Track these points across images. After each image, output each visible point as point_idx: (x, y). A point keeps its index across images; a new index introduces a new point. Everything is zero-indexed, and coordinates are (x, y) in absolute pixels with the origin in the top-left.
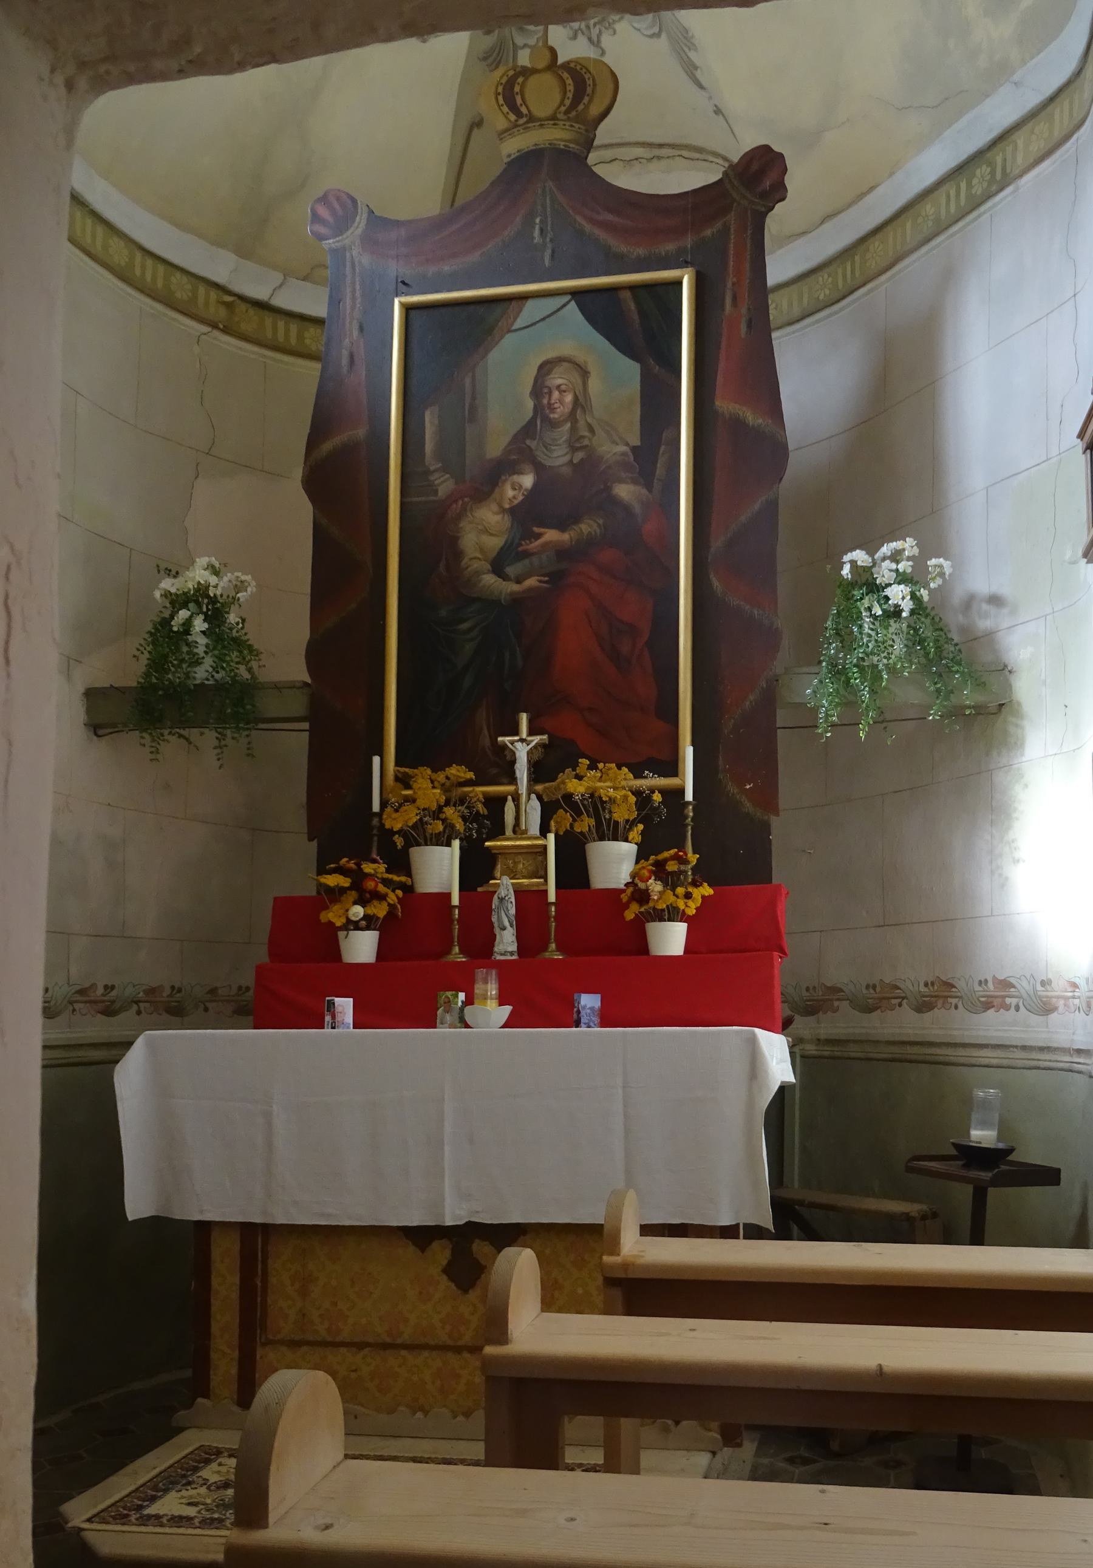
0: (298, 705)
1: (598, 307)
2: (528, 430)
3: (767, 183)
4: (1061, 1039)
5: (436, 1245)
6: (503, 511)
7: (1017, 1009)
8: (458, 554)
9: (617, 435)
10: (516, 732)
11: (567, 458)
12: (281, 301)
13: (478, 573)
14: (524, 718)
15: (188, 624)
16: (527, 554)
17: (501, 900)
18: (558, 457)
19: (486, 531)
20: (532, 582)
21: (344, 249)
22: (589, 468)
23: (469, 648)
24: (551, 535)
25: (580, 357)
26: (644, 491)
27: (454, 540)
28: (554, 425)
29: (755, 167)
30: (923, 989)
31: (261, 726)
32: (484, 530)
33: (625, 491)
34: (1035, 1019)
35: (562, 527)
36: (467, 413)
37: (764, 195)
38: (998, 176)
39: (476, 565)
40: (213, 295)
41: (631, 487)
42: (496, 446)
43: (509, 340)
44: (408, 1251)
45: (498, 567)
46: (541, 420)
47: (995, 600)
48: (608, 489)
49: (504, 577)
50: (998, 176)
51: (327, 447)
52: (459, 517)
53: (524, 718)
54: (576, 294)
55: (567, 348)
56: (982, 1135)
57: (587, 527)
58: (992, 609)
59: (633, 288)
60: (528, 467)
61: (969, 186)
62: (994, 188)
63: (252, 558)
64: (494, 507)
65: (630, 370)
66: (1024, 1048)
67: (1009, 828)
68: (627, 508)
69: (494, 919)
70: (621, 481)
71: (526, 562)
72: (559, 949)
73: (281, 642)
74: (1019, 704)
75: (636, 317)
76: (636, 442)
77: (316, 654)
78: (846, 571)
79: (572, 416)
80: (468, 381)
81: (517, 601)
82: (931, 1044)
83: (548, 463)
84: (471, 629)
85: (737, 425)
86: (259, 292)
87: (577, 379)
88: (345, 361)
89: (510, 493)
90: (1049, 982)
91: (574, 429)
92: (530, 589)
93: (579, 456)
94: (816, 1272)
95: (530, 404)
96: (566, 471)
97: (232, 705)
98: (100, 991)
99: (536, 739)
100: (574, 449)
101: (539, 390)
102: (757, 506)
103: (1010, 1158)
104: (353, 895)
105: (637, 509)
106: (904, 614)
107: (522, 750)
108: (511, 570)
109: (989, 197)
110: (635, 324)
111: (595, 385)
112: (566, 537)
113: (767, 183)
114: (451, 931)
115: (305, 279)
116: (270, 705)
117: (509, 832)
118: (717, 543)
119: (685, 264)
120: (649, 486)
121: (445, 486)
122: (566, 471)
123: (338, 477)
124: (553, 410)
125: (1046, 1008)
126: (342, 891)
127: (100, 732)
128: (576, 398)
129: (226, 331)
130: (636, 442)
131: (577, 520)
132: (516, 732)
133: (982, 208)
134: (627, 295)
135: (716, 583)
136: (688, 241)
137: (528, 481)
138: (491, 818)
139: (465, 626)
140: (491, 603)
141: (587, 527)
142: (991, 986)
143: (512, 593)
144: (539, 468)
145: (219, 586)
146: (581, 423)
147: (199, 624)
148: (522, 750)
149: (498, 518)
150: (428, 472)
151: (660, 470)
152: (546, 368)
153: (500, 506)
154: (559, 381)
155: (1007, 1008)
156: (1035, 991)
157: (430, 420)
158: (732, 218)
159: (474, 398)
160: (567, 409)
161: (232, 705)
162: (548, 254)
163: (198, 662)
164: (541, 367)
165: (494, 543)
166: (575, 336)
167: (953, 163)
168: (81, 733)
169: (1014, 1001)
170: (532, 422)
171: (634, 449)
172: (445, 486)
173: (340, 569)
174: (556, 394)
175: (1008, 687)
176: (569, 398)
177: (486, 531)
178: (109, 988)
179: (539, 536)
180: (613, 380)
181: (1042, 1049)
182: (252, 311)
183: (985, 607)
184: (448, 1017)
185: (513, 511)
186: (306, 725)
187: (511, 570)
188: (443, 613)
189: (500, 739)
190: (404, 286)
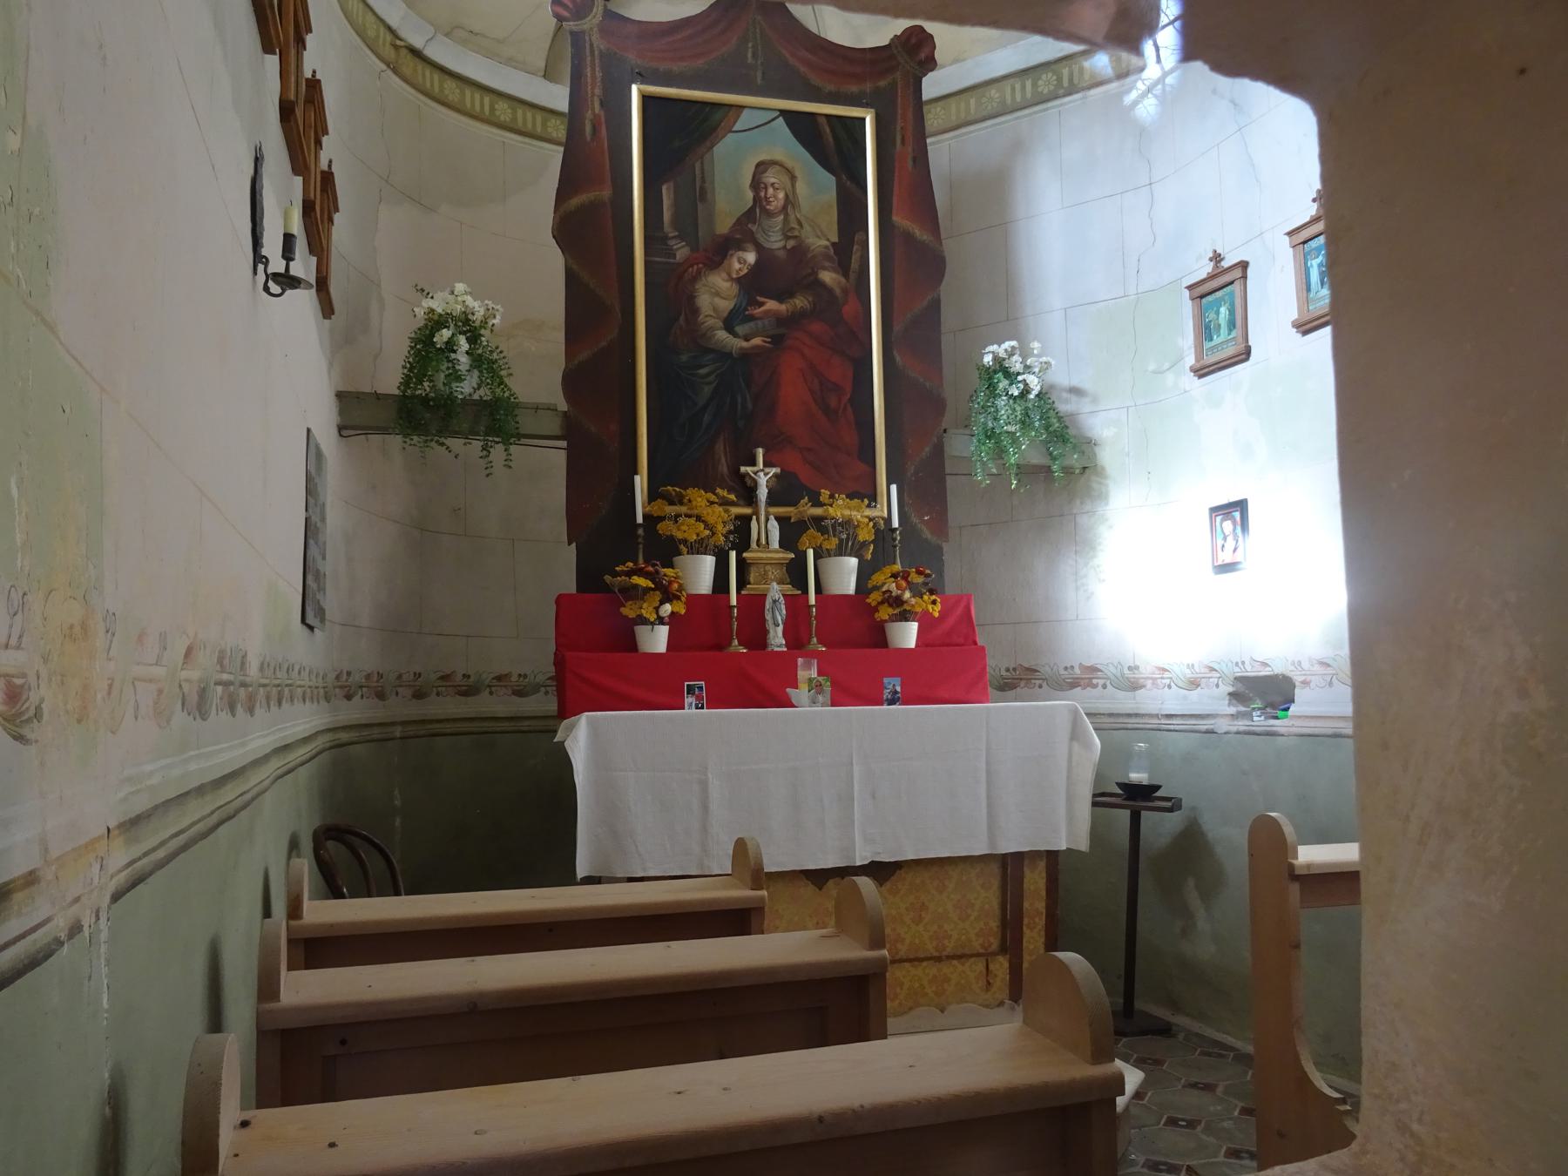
0: (553, 425)
1: (802, 126)
2: (749, 215)
3: (923, 56)
4: (1151, 708)
5: (831, 883)
6: (732, 279)
7: (1104, 686)
8: (695, 311)
9: (821, 234)
10: (753, 463)
11: (781, 244)
12: (432, 52)
13: (712, 329)
14: (760, 452)
15: (450, 346)
16: (752, 318)
17: (775, 601)
18: (775, 241)
19: (717, 294)
20: (757, 341)
21: (583, 32)
22: (798, 253)
23: (707, 390)
24: (771, 305)
25: (789, 163)
26: (843, 280)
27: (691, 298)
28: (770, 214)
29: (913, 40)
30: (1004, 673)
31: (523, 441)
32: (716, 294)
33: (828, 277)
34: (1121, 694)
35: (781, 301)
36: (696, 196)
37: (921, 63)
38: (1066, 84)
39: (711, 322)
40: (389, 37)
41: (834, 275)
42: (724, 226)
43: (730, 138)
44: (808, 890)
45: (729, 324)
46: (757, 211)
47: (1076, 391)
48: (815, 273)
49: (735, 335)
50: (1066, 84)
51: (575, 202)
52: (696, 278)
53: (760, 452)
54: (784, 113)
55: (778, 155)
56: (1138, 777)
57: (800, 302)
58: (1074, 398)
59: (828, 116)
60: (750, 246)
61: (1035, 85)
62: (1061, 92)
63: (513, 288)
64: (724, 275)
65: (829, 180)
66: (1111, 715)
67: (1094, 557)
68: (829, 290)
69: (768, 617)
70: (825, 268)
71: (752, 324)
72: (820, 642)
73: (537, 371)
74: (1103, 469)
75: (831, 139)
76: (835, 239)
77: (572, 381)
78: (988, 359)
79: (785, 208)
80: (698, 165)
81: (745, 356)
82: (1143, 716)
83: (767, 245)
84: (708, 375)
85: (908, 237)
86: (417, 42)
87: (786, 179)
88: (588, 129)
89: (737, 266)
90: (1137, 668)
91: (786, 220)
92: (757, 347)
93: (791, 244)
94: (421, 921)
95: (750, 195)
96: (782, 254)
97: (496, 419)
98: (459, 677)
99: (773, 471)
100: (788, 238)
101: (757, 184)
102: (925, 303)
103: (1158, 794)
104: (658, 596)
105: (838, 291)
106: (1032, 396)
107: (763, 478)
108: (739, 329)
109: (1057, 97)
110: (833, 147)
111: (801, 187)
112: (783, 307)
113: (923, 56)
114: (810, 625)
115: (446, 35)
116: (527, 423)
117: (754, 545)
118: (897, 328)
119: (866, 105)
120: (846, 274)
121: (682, 252)
122: (782, 254)
123: (586, 228)
124: (769, 203)
125: (1134, 686)
126: (648, 589)
127: (345, 433)
128: (787, 196)
129: (395, 71)
130: (835, 239)
131: (792, 295)
132: (753, 463)
133: (1050, 104)
134: (823, 121)
135: (898, 359)
136: (868, 87)
137: (751, 257)
138: (741, 534)
139: (703, 371)
140: (724, 355)
141: (800, 302)
142: (1077, 671)
143: (741, 348)
144: (759, 249)
145: (478, 308)
146: (792, 217)
147: (463, 344)
148: (763, 478)
149: (728, 285)
150: (665, 238)
151: (855, 265)
152: (762, 167)
153: (729, 274)
154: (773, 180)
155: (1095, 686)
156: (1123, 675)
157: (667, 193)
158: (898, 75)
159: (703, 181)
160: (782, 202)
161: (496, 419)
162: (759, 74)
163: (459, 379)
164: (758, 165)
165: (726, 305)
166: (784, 146)
167: (1023, 66)
168: (335, 431)
169: (1101, 682)
170: (751, 211)
171: (833, 244)
172: (682, 252)
173: (591, 309)
174: (771, 191)
175: (1093, 457)
176: (781, 195)
177: (717, 294)
178: (418, 675)
179: (762, 304)
180: (815, 188)
181: (1129, 715)
182: (409, 56)
183: (1065, 395)
184: (820, 698)
185: (739, 280)
186: (564, 444)
187: (739, 329)
188: (684, 358)
189: (743, 469)
190: (642, 77)
